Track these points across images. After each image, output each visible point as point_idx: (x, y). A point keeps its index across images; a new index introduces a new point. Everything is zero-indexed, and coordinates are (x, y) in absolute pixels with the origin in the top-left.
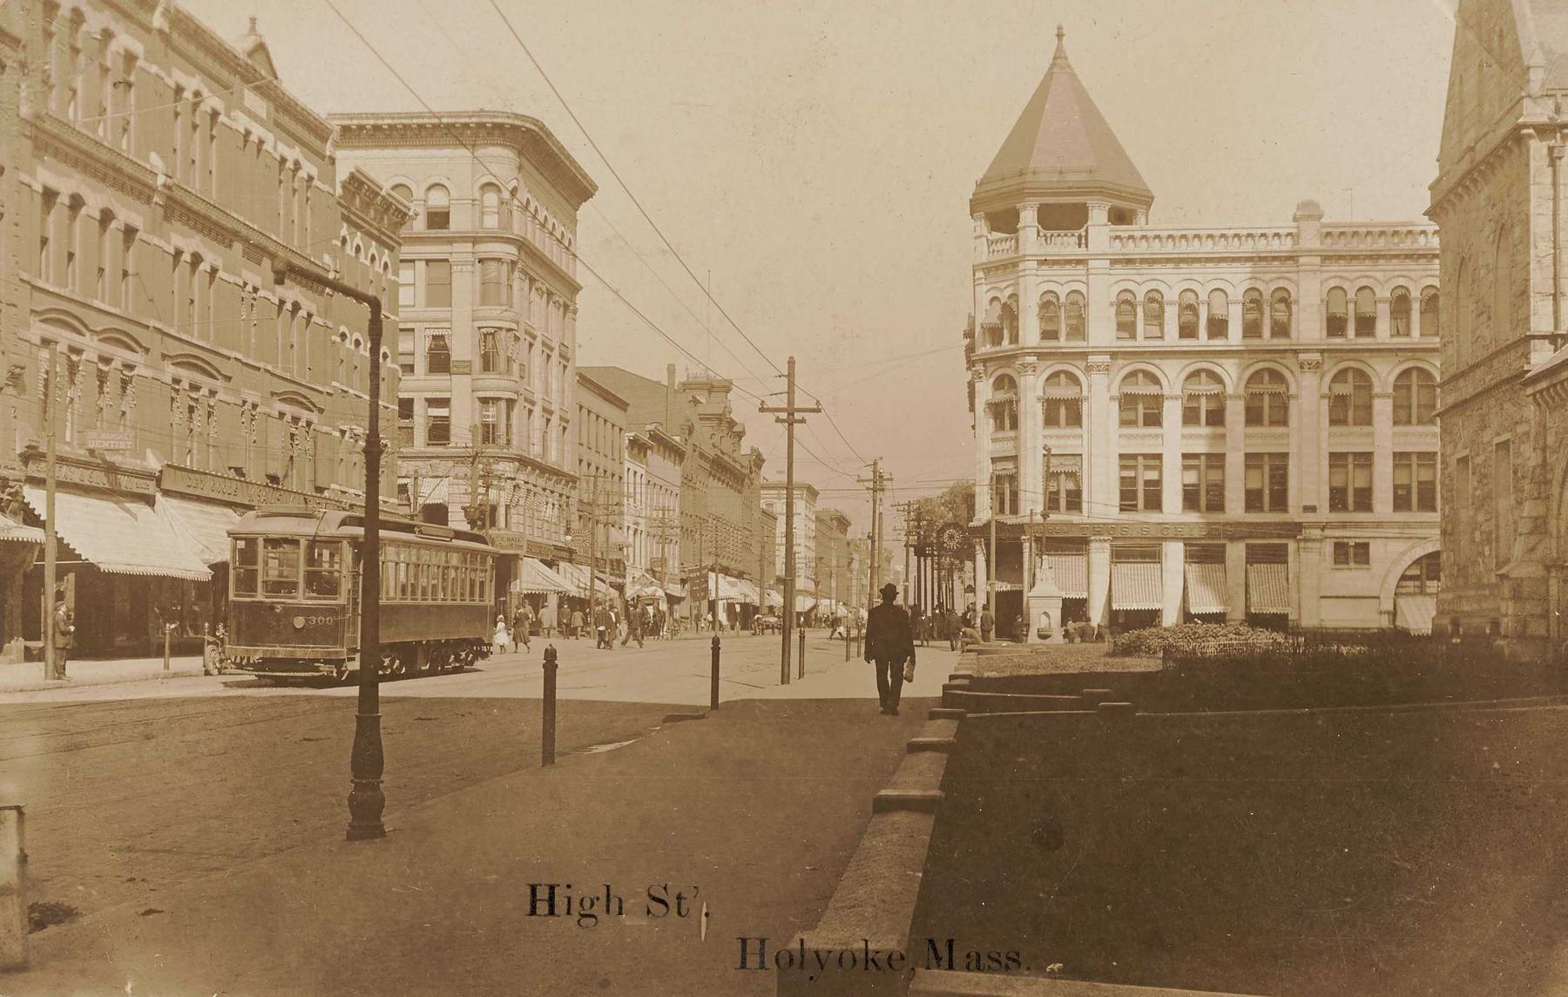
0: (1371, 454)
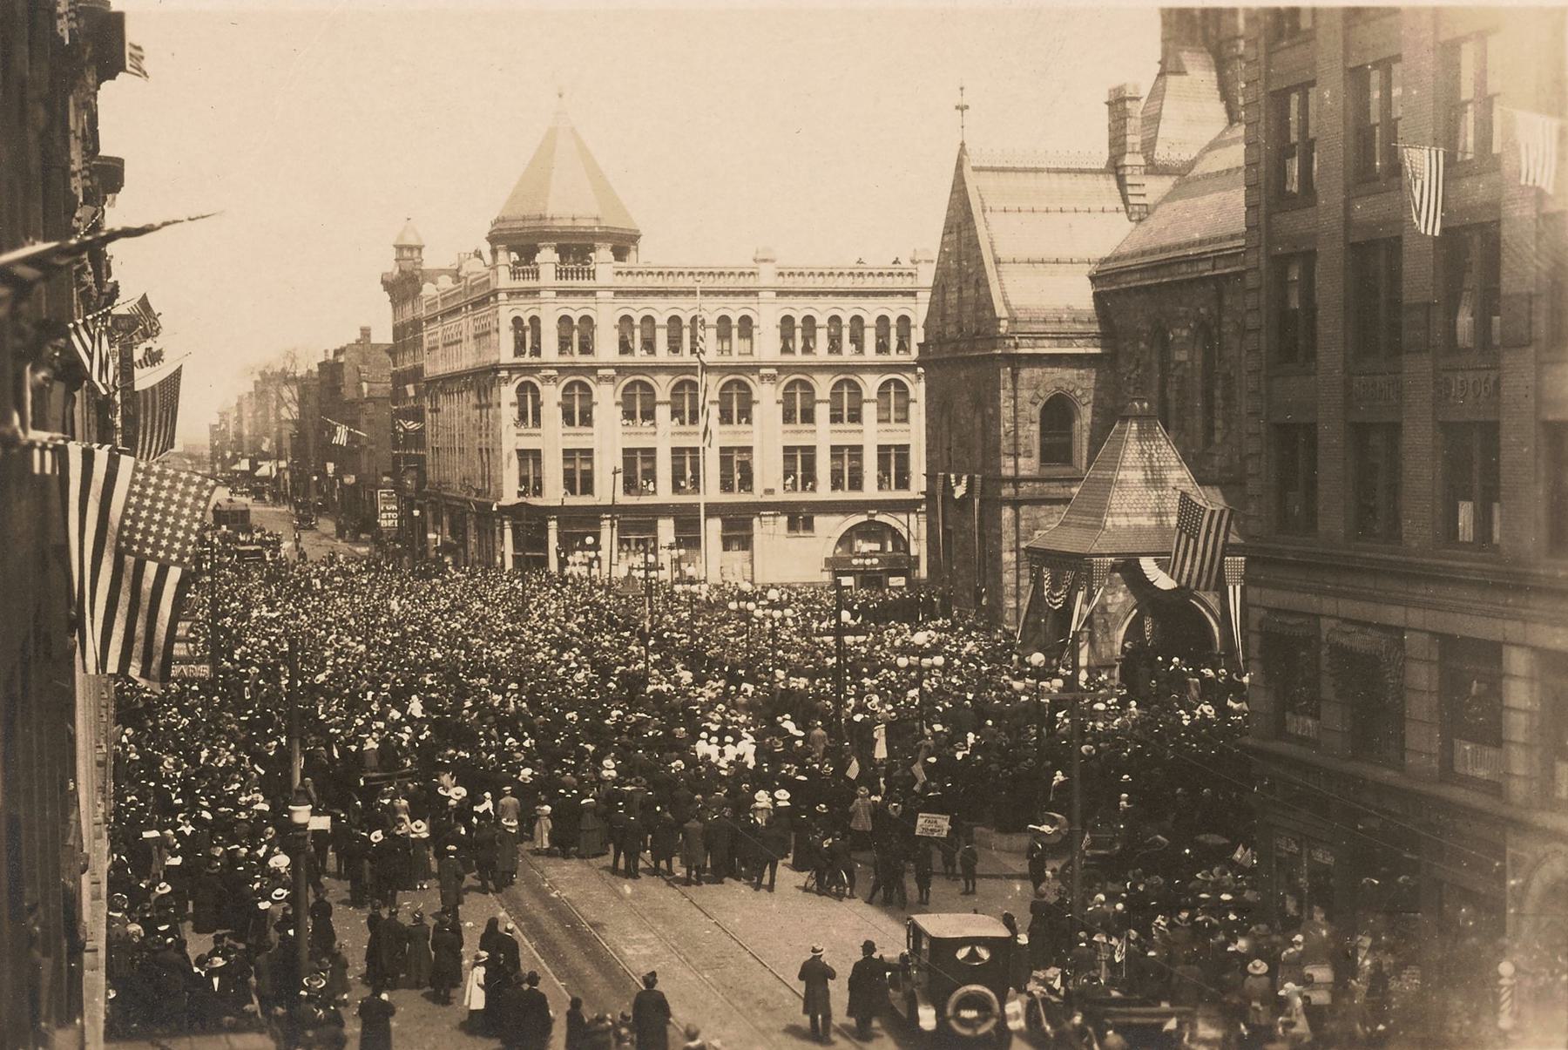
0: (814, 447)
